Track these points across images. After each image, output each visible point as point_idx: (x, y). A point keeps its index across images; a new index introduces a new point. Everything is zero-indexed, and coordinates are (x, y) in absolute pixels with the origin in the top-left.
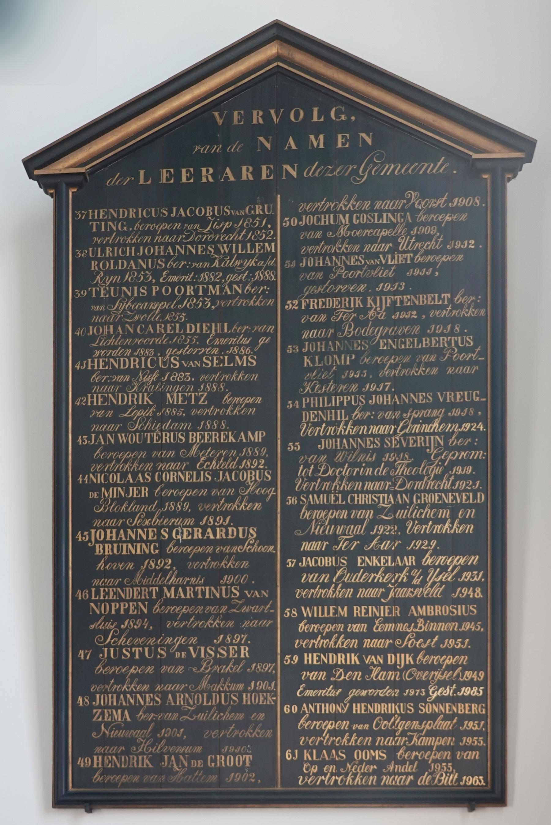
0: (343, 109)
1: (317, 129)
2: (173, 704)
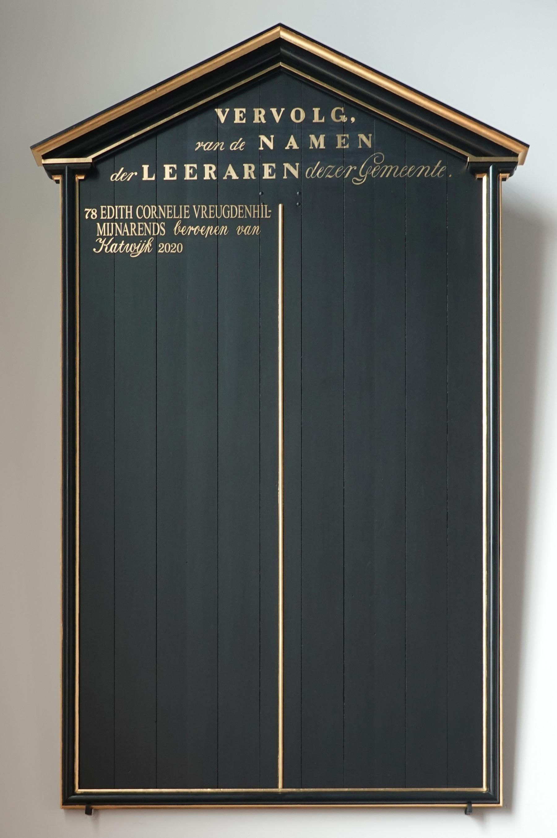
0: (342, 109)
1: (318, 129)
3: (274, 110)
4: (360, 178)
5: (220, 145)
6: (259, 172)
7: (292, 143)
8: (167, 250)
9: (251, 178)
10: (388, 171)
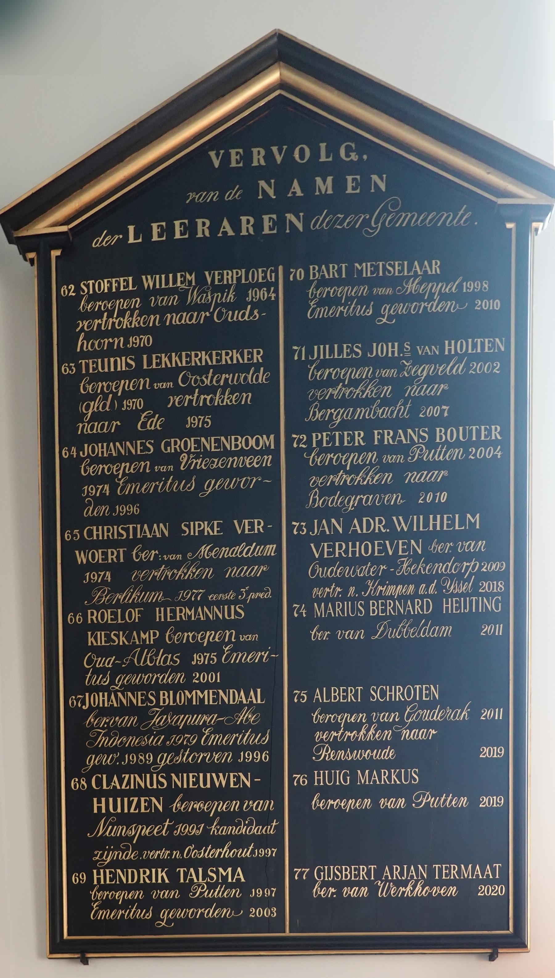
0: (353, 145)
1: (323, 170)
2: (378, 783)
3: (275, 149)
4: (372, 228)
5: (213, 196)
8: (488, 892)
9: (249, 234)
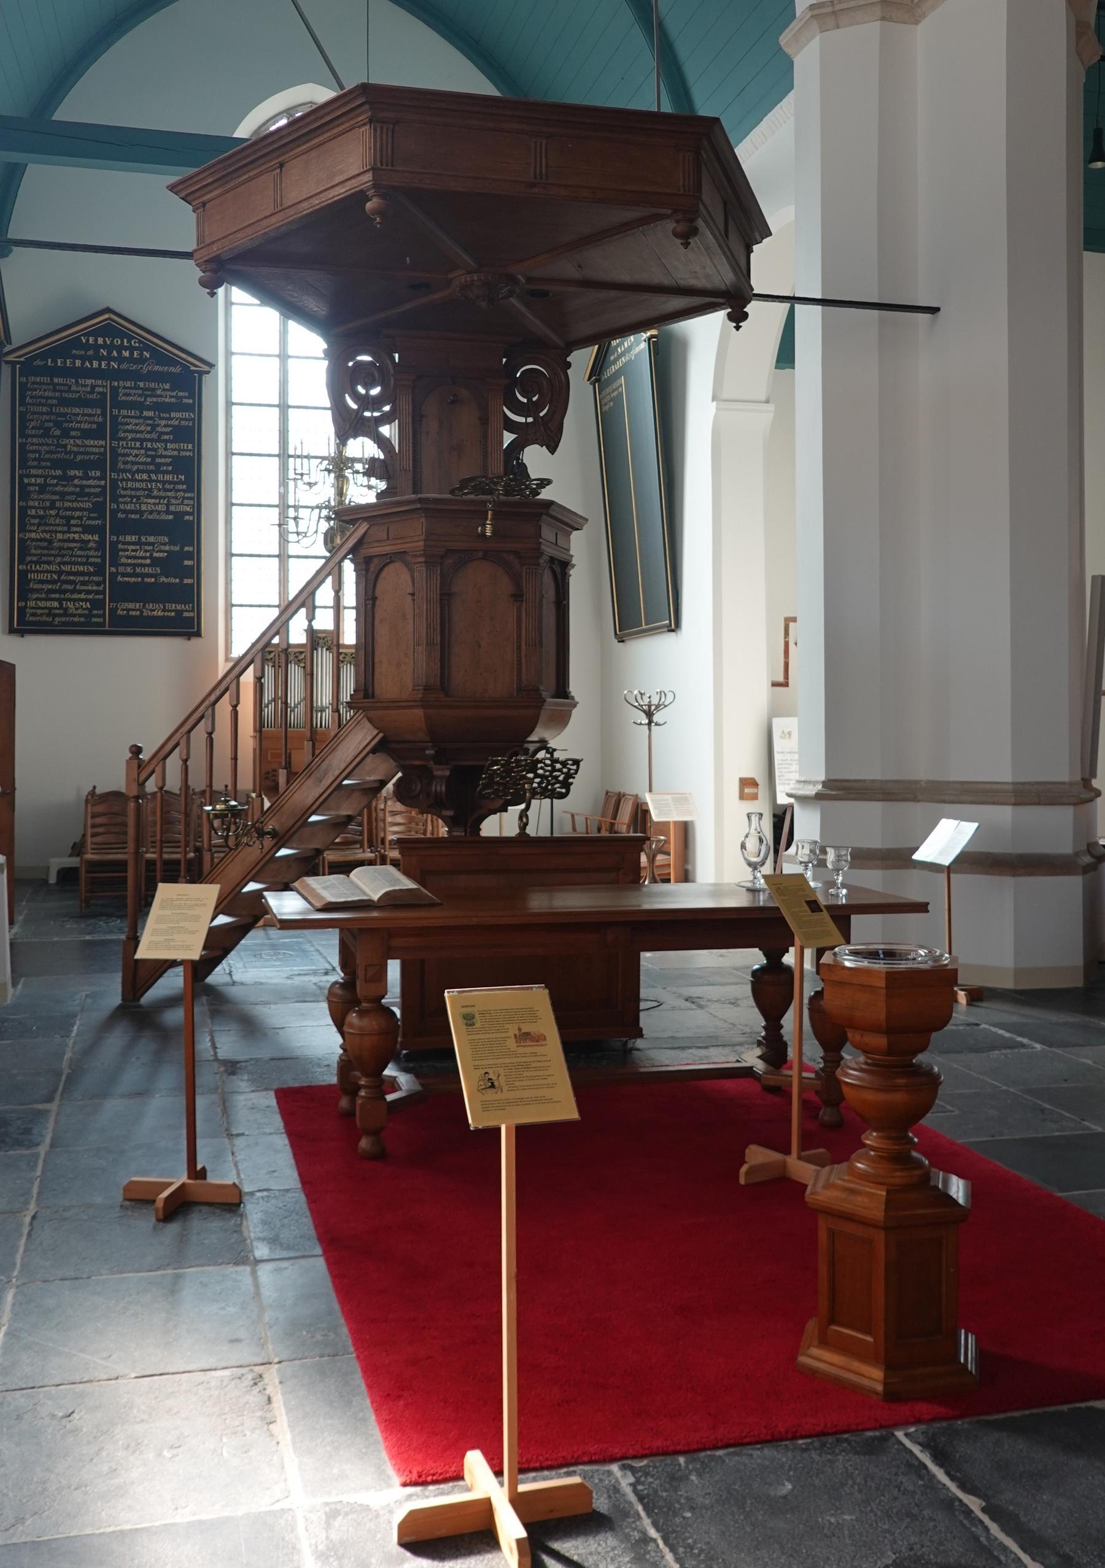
6: (100, 365)
7: (115, 353)
10: (157, 368)
